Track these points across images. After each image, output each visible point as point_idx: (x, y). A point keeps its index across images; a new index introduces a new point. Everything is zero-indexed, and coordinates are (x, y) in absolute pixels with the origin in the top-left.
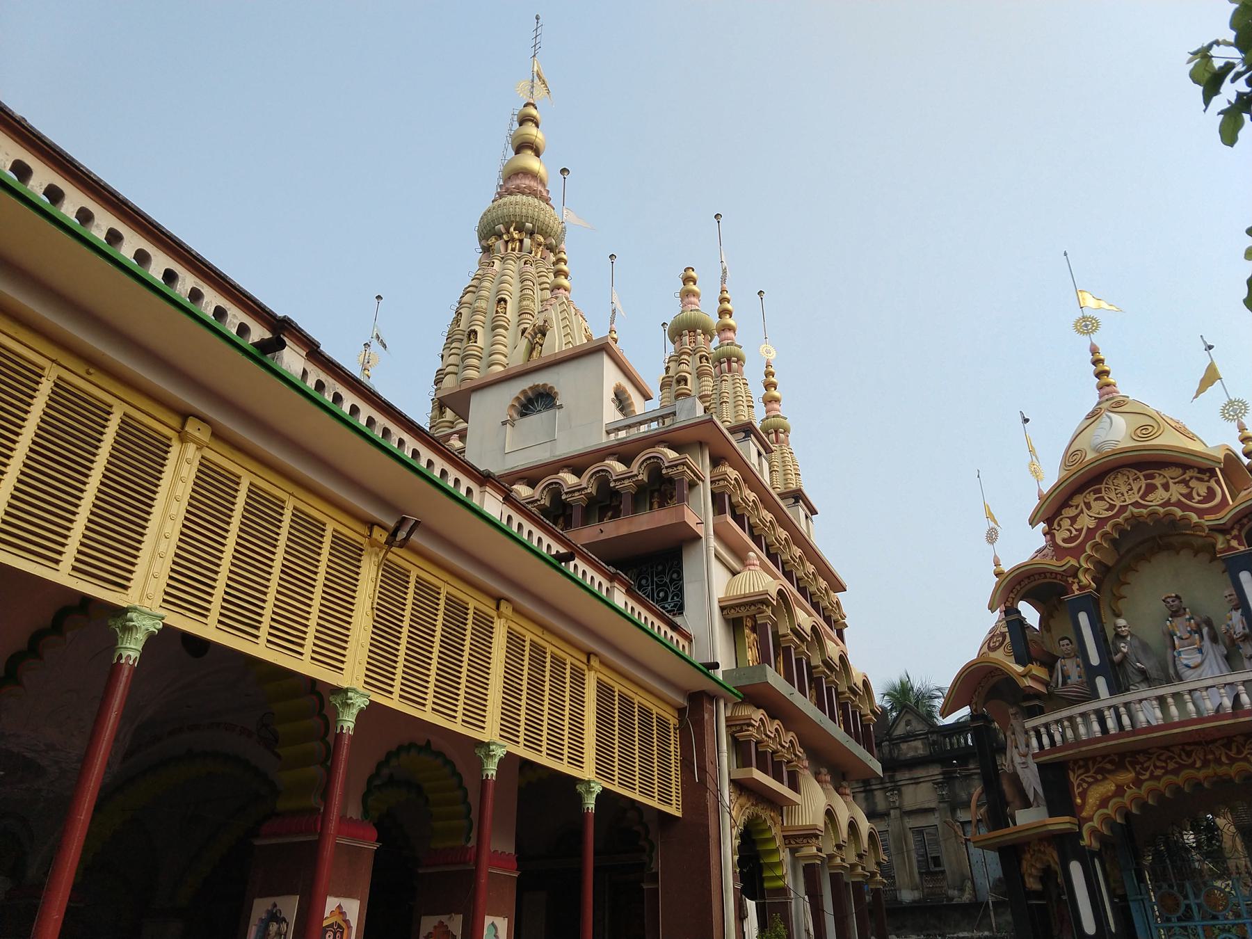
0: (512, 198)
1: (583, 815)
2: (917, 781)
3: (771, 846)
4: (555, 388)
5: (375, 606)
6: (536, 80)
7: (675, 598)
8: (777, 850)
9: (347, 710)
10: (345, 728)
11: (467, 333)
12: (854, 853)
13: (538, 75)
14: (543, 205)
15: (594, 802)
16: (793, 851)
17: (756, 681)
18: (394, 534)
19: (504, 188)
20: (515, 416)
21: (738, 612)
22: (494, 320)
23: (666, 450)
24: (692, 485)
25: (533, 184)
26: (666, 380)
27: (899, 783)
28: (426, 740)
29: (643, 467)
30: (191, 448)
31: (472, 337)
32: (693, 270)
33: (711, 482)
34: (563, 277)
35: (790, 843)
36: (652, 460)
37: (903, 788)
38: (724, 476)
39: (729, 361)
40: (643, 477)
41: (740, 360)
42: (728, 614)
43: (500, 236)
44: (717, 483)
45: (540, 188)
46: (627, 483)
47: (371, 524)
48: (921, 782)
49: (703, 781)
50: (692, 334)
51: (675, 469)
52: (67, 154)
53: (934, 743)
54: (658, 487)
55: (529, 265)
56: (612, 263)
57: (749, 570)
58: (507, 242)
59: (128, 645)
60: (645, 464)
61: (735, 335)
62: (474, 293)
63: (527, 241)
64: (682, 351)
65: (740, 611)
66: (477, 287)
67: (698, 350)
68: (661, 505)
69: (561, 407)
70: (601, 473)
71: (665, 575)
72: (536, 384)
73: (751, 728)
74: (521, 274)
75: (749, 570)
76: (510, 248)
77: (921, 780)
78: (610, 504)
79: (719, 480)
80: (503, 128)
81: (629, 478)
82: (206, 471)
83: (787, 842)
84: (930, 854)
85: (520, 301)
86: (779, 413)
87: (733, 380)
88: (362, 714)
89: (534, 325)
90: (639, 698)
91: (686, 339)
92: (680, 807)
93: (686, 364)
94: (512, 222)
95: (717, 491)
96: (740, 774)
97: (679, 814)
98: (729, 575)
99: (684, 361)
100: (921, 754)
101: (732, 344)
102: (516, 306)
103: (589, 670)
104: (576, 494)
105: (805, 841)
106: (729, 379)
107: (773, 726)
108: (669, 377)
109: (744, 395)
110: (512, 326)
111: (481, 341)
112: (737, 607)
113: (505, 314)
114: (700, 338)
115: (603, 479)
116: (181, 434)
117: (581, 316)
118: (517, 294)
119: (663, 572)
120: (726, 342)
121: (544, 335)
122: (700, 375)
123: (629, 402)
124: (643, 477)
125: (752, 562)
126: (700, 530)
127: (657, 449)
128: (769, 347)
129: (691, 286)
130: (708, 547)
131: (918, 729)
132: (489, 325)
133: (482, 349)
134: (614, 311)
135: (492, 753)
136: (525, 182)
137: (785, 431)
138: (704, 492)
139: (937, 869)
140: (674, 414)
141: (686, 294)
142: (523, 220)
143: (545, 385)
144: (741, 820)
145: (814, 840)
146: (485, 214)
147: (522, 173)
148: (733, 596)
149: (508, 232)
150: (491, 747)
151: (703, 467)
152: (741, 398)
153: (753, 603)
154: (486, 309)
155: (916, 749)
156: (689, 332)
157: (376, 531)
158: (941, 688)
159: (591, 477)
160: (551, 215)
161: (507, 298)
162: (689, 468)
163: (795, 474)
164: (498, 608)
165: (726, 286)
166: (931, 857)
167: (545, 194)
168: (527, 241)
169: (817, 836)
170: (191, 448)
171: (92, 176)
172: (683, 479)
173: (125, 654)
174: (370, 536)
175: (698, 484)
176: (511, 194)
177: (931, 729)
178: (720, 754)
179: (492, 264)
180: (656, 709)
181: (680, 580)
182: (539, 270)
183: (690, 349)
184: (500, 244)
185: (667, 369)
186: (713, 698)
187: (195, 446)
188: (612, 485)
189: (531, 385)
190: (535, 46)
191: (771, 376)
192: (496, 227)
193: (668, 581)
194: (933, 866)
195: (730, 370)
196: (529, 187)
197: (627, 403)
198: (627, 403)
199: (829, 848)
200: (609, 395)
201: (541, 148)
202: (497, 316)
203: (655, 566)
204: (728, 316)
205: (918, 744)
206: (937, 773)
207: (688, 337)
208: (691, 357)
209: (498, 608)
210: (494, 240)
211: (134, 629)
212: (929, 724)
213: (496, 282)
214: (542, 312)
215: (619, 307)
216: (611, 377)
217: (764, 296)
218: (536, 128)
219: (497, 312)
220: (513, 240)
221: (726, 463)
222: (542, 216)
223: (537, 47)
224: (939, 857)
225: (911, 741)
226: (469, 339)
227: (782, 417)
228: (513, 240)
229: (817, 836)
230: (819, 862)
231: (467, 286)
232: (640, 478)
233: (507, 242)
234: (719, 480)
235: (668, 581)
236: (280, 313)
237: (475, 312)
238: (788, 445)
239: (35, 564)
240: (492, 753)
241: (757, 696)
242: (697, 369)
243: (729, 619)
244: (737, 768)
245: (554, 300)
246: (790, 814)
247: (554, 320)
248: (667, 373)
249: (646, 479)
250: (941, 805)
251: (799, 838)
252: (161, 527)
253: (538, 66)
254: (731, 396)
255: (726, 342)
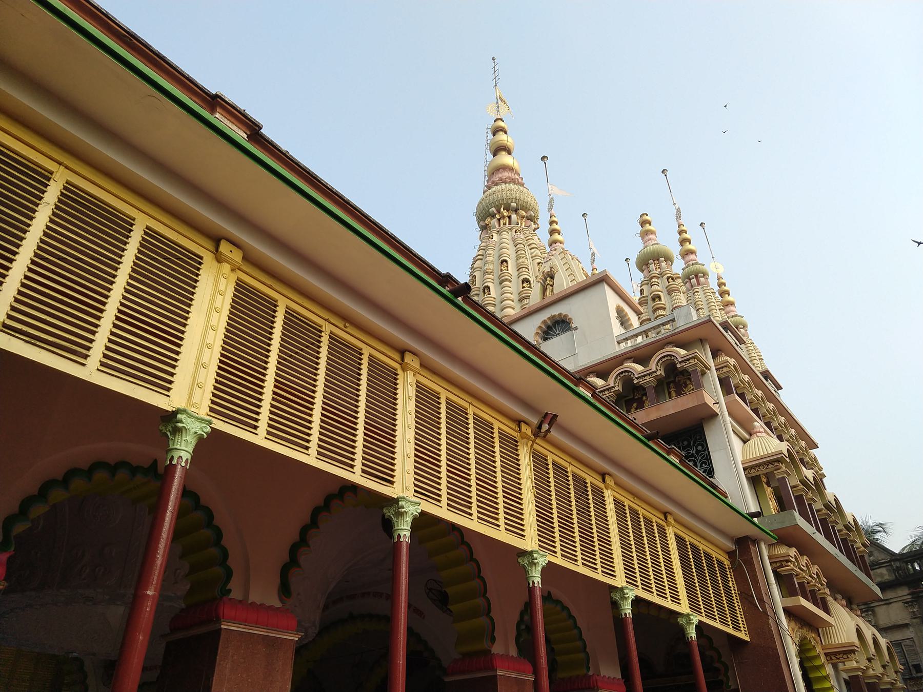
0: (499, 187)
1: (687, 643)
2: (888, 602)
3: (817, 663)
4: (569, 315)
5: (534, 485)
6: (500, 102)
7: (704, 465)
8: (823, 666)
9: (534, 568)
10: (536, 583)
11: (481, 289)
12: (879, 665)
13: (500, 98)
14: (521, 188)
15: (694, 632)
16: (835, 666)
17: (787, 524)
18: (540, 427)
19: (490, 181)
20: (540, 340)
21: (758, 471)
22: (500, 277)
23: (678, 349)
24: (703, 373)
25: (511, 175)
26: (641, 300)
27: (872, 605)
28: (547, 592)
29: (660, 365)
30: (410, 374)
31: (486, 291)
32: (647, 215)
33: (716, 369)
34: (557, 234)
35: (832, 659)
36: (666, 358)
37: (877, 609)
38: (726, 364)
39: (697, 277)
40: (661, 372)
41: (705, 274)
42: (749, 473)
43: (493, 216)
44: (721, 370)
45: (517, 177)
46: (648, 379)
47: (519, 422)
48: (891, 603)
49: (765, 612)
50: (656, 262)
51: (688, 362)
52: (313, 173)
53: (898, 569)
54: (673, 379)
55: (519, 233)
56: (585, 219)
57: (757, 436)
58: (499, 220)
59: (402, 527)
60: (661, 362)
61: (697, 256)
62: (482, 259)
63: (514, 217)
64: (651, 276)
65: (759, 470)
66: (483, 255)
67: (664, 273)
68: (679, 394)
69: (576, 328)
70: (624, 374)
71: (691, 448)
72: (553, 314)
73: (789, 564)
74: (514, 241)
75: (757, 436)
76: (502, 223)
77: (892, 601)
78: (633, 398)
79: (722, 368)
80: (482, 140)
81: (649, 374)
82: (421, 389)
83: (828, 658)
84: (911, 662)
85: (517, 260)
86: (736, 313)
87: (704, 294)
88: (544, 570)
89: (543, 272)
90: (703, 546)
91: (652, 266)
92: (747, 633)
93: (656, 285)
94: (501, 204)
95: (722, 377)
96: (791, 602)
97: (747, 639)
98: (742, 443)
99: (655, 283)
100: (887, 579)
101: (697, 263)
102: (515, 264)
103: (668, 526)
104: (606, 392)
105: (845, 656)
106: (700, 290)
107: (804, 560)
108: (644, 297)
109: (714, 301)
110: (514, 279)
111: (493, 294)
112: (756, 467)
113: (508, 270)
114: (664, 264)
115: (627, 380)
116: (402, 365)
117: (577, 260)
118: (513, 255)
119: (689, 446)
120: (691, 263)
121: (552, 278)
122: (670, 292)
123: (627, 318)
124: (661, 372)
125: (758, 430)
126: (716, 408)
127: (666, 349)
128: (719, 265)
129: (648, 227)
130: (725, 422)
131: (880, 559)
132: (497, 281)
133: (495, 298)
134: (593, 255)
135: (626, 596)
136: (506, 175)
137: (744, 327)
138: (712, 379)
139: (919, 675)
140: (673, 320)
141: (645, 234)
142: (509, 202)
143: (560, 314)
144: (797, 640)
145: (853, 655)
146: (478, 206)
147: (502, 168)
148: (750, 459)
149: (499, 212)
150: (625, 591)
151: (706, 356)
152: (713, 304)
153: (770, 462)
154: (493, 270)
155: (881, 575)
156: (654, 261)
157: (524, 427)
158: (881, 524)
159: (616, 378)
160: (529, 195)
161: (508, 259)
162: (699, 360)
163: (759, 359)
164: (604, 481)
165: (682, 221)
166: (912, 665)
167: (520, 181)
168: (514, 217)
169: (853, 652)
170: (410, 374)
171: (328, 186)
172: (696, 369)
173: (402, 533)
174: (520, 430)
175: (706, 373)
176: (497, 184)
177: (893, 558)
178: (770, 587)
179: (491, 237)
180: (716, 554)
181: (705, 450)
182: (526, 235)
183: (657, 274)
184: (494, 222)
185: (642, 292)
186: (755, 541)
187: (412, 373)
188: (635, 381)
189: (549, 316)
190: (495, 78)
191: (723, 286)
192: (490, 210)
193: (694, 453)
194: (915, 673)
195: (699, 284)
196: (509, 178)
197: (625, 319)
198: (625, 319)
199: (863, 664)
200: (613, 314)
201: (511, 148)
202: (502, 273)
203: (680, 443)
204: (688, 243)
205: (883, 571)
206: (906, 594)
207: (653, 264)
208: (660, 279)
209: (604, 481)
210: (489, 220)
211: (405, 514)
212: (891, 554)
213: (497, 249)
214: (547, 261)
215: (594, 249)
216: (613, 301)
217: (705, 226)
218: (506, 135)
219: (502, 270)
220: (503, 217)
221: (723, 353)
222: (522, 196)
223: (497, 79)
224: (919, 664)
225: (876, 569)
226: (484, 293)
227: (739, 316)
228: (503, 217)
229: (853, 652)
230: (860, 674)
231: (476, 255)
232: (658, 373)
233: (499, 220)
234: (722, 368)
235: (694, 453)
236: (443, 271)
237: (485, 273)
238: (748, 337)
239: (342, 469)
240: (626, 596)
241: (788, 537)
242: (666, 288)
243: (749, 478)
244: (783, 597)
245: (554, 252)
246: (826, 634)
247: (558, 265)
248: (641, 294)
249: (663, 374)
250: (914, 621)
251: (839, 654)
252: (404, 435)
253: (499, 92)
254: (705, 303)
255: (691, 263)
